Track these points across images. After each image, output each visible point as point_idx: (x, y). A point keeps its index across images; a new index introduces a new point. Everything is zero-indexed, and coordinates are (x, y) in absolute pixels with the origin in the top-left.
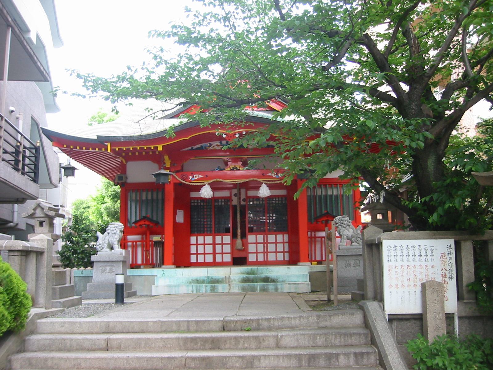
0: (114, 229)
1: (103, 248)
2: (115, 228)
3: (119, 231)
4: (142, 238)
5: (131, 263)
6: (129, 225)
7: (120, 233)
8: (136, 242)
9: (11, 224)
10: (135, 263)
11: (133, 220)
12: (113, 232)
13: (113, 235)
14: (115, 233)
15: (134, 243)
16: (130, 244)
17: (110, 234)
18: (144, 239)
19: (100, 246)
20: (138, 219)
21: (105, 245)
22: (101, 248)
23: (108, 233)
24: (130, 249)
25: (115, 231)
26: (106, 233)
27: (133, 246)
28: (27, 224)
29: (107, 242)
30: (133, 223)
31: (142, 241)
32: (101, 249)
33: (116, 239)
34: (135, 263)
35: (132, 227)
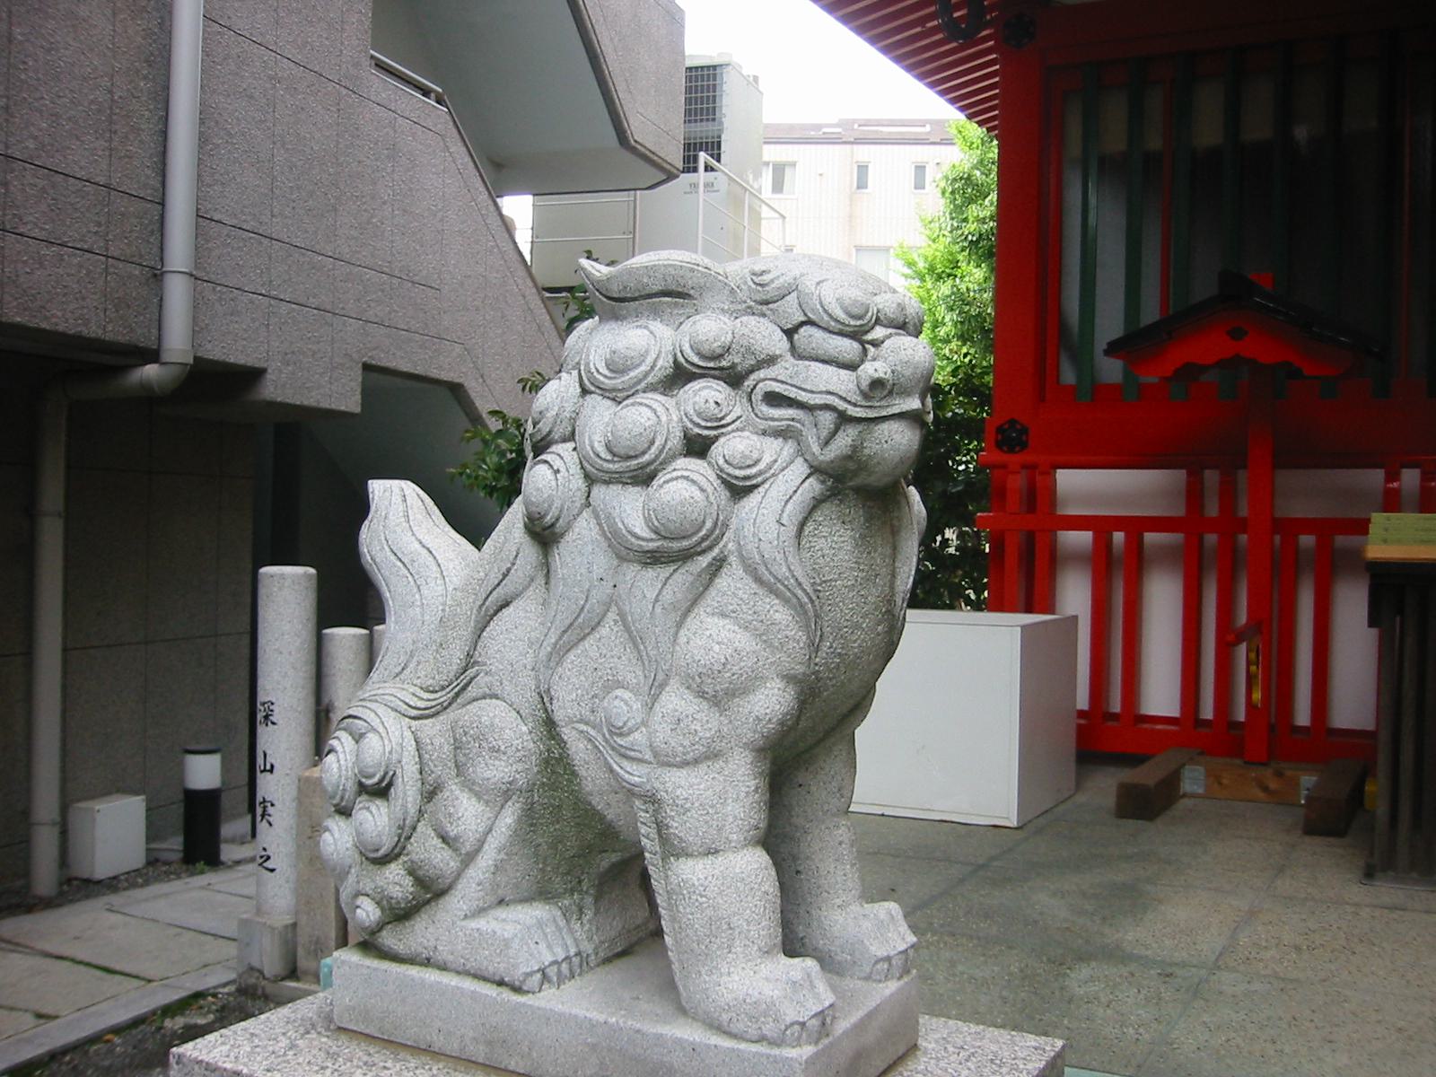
0: (654, 418)
1: (430, 891)
2: (706, 394)
3: (788, 484)
4: (1194, 495)
5: (1082, 702)
6: (1068, 376)
7: (836, 541)
8: (1136, 526)
9: (150, 371)
10: (1116, 706)
11: (1110, 325)
12: (630, 510)
13: (647, 583)
14: (679, 550)
15: (1119, 537)
16: (1080, 539)
17: (582, 548)
18: (1212, 509)
19: (376, 820)
20: (1150, 313)
21: (467, 813)
22: (395, 880)
23: (544, 535)
24: (1075, 595)
25: (686, 488)
26: (511, 526)
27: (1102, 564)
28: (367, 368)
29: (504, 726)
30: (1113, 349)
31: (1189, 523)
32: (400, 914)
33: (719, 692)
34: (1116, 706)
35: (1105, 394)
